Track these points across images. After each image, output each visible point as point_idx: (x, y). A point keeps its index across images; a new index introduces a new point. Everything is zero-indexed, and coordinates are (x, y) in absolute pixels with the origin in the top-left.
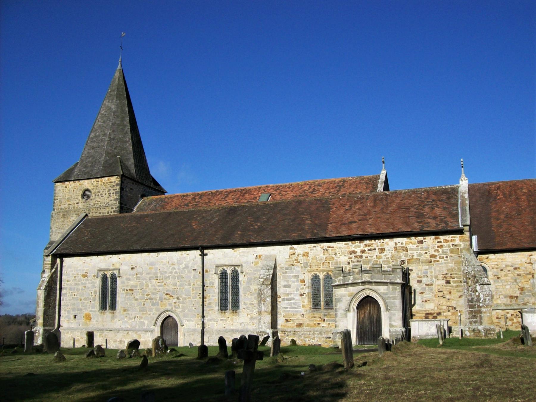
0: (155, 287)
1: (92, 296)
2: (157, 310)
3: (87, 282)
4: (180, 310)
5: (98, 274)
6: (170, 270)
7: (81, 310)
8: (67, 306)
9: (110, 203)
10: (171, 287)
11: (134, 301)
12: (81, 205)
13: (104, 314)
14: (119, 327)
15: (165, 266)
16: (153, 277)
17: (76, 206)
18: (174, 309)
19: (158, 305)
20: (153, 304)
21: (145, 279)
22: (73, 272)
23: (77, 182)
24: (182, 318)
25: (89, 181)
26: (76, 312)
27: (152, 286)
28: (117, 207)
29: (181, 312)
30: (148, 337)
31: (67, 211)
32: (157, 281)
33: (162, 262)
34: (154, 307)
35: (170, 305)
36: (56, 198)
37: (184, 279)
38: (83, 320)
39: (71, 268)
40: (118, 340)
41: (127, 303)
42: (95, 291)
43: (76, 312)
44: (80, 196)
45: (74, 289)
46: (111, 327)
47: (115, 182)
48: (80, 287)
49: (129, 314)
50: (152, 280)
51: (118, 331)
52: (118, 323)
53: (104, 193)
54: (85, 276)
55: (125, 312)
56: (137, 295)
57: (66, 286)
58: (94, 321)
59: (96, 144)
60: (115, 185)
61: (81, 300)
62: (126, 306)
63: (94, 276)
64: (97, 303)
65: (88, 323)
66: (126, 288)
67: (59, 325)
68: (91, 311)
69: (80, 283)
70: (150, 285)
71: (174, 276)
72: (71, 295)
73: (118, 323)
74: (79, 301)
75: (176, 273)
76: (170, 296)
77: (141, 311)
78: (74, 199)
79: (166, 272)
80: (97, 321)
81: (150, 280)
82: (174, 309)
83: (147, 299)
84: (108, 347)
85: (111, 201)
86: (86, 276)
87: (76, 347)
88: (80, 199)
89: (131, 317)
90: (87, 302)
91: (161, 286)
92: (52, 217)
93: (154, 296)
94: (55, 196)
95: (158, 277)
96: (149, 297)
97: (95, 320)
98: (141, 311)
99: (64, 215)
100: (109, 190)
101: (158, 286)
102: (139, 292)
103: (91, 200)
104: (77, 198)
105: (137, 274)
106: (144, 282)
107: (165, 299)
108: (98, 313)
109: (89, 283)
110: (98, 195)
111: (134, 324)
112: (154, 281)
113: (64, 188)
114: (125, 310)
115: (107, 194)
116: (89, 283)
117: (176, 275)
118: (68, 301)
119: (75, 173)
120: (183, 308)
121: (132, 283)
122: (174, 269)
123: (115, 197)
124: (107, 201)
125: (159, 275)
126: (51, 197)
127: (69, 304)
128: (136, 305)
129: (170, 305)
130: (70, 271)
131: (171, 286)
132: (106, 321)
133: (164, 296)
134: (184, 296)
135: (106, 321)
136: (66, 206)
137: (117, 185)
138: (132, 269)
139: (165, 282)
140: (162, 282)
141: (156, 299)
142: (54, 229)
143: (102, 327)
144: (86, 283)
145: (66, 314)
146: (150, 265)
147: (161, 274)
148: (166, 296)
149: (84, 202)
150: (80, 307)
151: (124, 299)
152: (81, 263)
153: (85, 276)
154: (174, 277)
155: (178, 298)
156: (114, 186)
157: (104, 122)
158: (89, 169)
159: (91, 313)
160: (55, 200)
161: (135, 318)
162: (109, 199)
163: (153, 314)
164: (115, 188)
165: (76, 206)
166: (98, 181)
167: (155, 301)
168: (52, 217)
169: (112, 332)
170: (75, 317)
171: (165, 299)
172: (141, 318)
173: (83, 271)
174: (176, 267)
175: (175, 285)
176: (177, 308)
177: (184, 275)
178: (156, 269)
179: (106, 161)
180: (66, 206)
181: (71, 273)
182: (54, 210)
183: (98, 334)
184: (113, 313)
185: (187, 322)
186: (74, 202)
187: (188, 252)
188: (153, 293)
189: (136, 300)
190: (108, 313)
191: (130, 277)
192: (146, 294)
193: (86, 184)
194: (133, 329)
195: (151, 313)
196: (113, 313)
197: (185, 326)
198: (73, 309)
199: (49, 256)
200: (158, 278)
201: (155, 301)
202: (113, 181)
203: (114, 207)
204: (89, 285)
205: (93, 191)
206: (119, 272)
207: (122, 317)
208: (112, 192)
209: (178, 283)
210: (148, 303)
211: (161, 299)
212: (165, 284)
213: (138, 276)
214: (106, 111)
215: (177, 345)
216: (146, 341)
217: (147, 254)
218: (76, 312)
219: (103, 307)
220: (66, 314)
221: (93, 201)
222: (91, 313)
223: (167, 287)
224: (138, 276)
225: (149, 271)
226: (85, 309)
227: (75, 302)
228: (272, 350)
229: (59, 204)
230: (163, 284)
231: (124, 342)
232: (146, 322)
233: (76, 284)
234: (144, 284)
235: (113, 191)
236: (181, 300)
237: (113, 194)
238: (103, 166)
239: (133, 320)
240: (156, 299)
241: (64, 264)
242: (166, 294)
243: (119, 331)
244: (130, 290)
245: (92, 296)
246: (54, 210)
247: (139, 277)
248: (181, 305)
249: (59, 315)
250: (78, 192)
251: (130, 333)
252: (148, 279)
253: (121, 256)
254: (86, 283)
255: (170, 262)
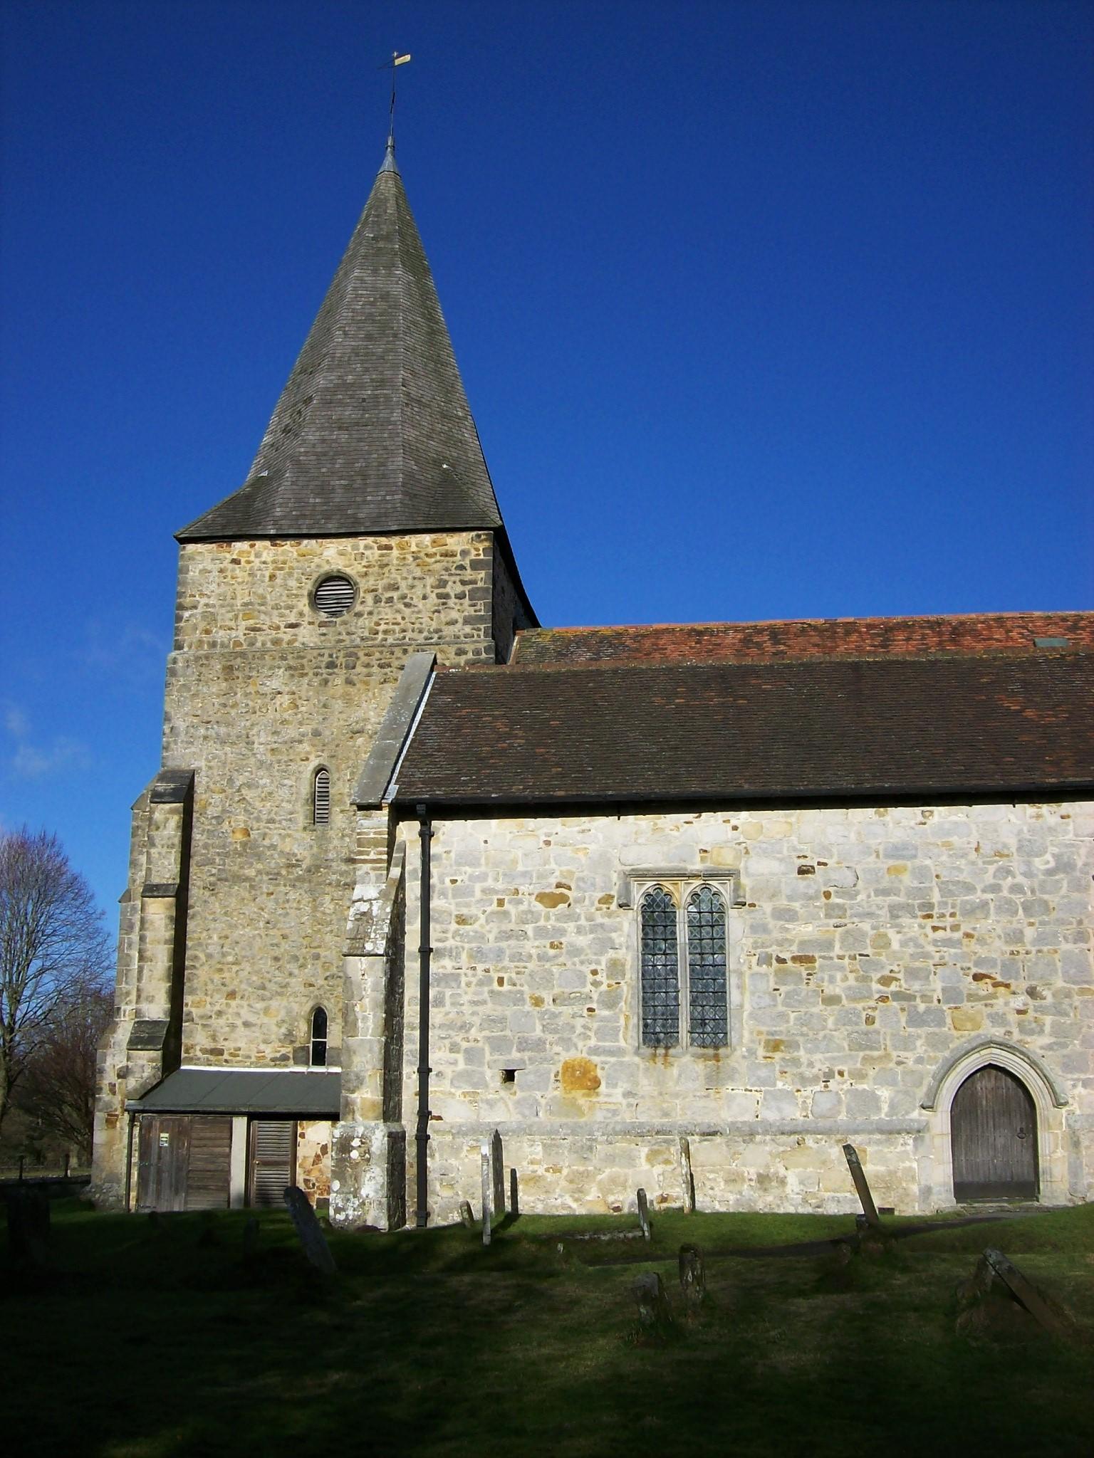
0: (917, 945)
1: (596, 984)
2: (936, 1042)
3: (570, 927)
4: (1046, 1040)
5: (626, 889)
6: (989, 879)
7: (539, 1045)
8: (465, 1027)
9: (449, 631)
10: (997, 949)
11: (818, 1008)
12: (307, 635)
13: (667, 1064)
14: (749, 1118)
15: (961, 863)
16: (908, 909)
17: (286, 635)
18: (1016, 1035)
19: (941, 1023)
20: (916, 1020)
21: (870, 915)
22: (490, 883)
23: (288, 546)
24: (1055, 1072)
25: (347, 543)
26: (515, 1055)
27: (904, 944)
28: (482, 646)
29: (1049, 1047)
30: (903, 1156)
31: (243, 655)
32: (930, 923)
33: (948, 845)
34: (923, 1031)
35: (998, 1019)
36: (187, 601)
37: (1054, 915)
38: (554, 1092)
39: (474, 863)
40: (752, 1172)
41: (783, 1017)
42: (615, 968)
43: (515, 1055)
44: (305, 601)
45: (500, 954)
46: (709, 1119)
47: (464, 553)
48: (531, 946)
49: (796, 1062)
50: (905, 920)
51: (749, 1133)
52: (740, 1102)
53: (419, 591)
54: (551, 900)
55: (778, 1055)
56: (832, 980)
57: (450, 943)
58: (612, 1094)
59: (349, 413)
60: (467, 563)
61: (538, 1002)
62: (783, 1028)
63: (607, 899)
64: (627, 1018)
65: (582, 1101)
66: (774, 950)
67: (424, 1115)
68: (595, 1051)
69: (529, 929)
70: (895, 939)
71: (1009, 902)
72: (481, 983)
73: (740, 1102)
74: (528, 1007)
75: (1017, 889)
76: (996, 985)
77: (856, 1046)
78: (276, 607)
79: (970, 888)
80: (628, 1094)
81: (894, 917)
82: (1016, 1035)
83: (884, 999)
84: (698, 1205)
85: (454, 622)
86: (563, 899)
87: (705, 1203)
88: (307, 610)
89: (809, 1073)
90: (567, 1010)
91: (949, 943)
92: (173, 673)
93: (916, 986)
94: (181, 595)
95: (931, 906)
96: (893, 987)
97: (619, 1091)
98: (856, 1046)
99: (229, 669)
100: (443, 584)
101: (935, 943)
102: (842, 968)
103: (359, 615)
104: (290, 608)
105: (827, 895)
106: (866, 926)
107: (972, 997)
108: (631, 1058)
109: (579, 931)
110: (390, 600)
111: (825, 1103)
112: (913, 925)
113: (226, 564)
114: (775, 1046)
115: (433, 598)
116: (579, 931)
117: (1018, 899)
118: (467, 1009)
119: (278, 512)
120: (1058, 1030)
121: (806, 930)
122: (1008, 872)
123: (471, 611)
124: (434, 625)
125: (936, 897)
126: (165, 603)
127: (476, 1020)
128: (830, 1022)
129: (998, 1019)
130: (472, 878)
131: (998, 943)
132: (677, 1095)
133: (968, 983)
134: (1059, 983)
135: (677, 1095)
136: (240, 634)
137: (475, 565)
138: (802, 871)
139: (965, 928)
140: (955, 928)
141: (926, 998)
142: (181, 724)
143: (658, 1121)
144: (563, 932)
145: (461, 1066)
146: (887, 856)
147: (945, 892)
148: (974, 985)
149: (321, 625)
150: (538, 1032)
151: (767, 1000)
152: (530, 844)
153: (551, 900)
154: (1008, 908)
155: (1032, 992)
156: (462, 567)
157: (369, 337)
158: (338, 497)
159: (595, 1059)
160: (181, 607)
161: (828, 1077)
162: (444, 617)
163: (919, 1060)
164: (469, 574)
165: (287, 638)
166: (389, 548)
167: (922, 1007)
168: (173, 673)
169: (718, 1139)
170: (509, 1076)
171: (972, 997)
172: (859, 1076)
173: (541, 876)
174: (1016, 864)
175: (1017, 937)
176: (1032, 1032)
177: (1053, 900)
178: (921, 873)
179: (410, 475)
180: (240, 634)
181: (478, 887)
182: (179, 647)
183: (644, 1151)
184: (717, 1058)
185: (1080, 1090)
186: (276, 620)
187: (1066, 807)
188: (912, 974)
189: (831, 1000)
190: (687, 1062)
191: (796, 905)
192: (876, 976)
193: (333, 554)
194: (822, 1123)
195: (910, 1057)
196: (717, 1058)
197: (1075, 1107)
198: (498, 1045)
199: (378, 807)
200: (935, 912)
201: (922, 1007)
202: (458, 549)
203: (469, 648)
204: (583, 941)
205: (363, 584)
206: (738, 886)
207: (763, 1073)
208: (453, 588)
209: (1030, 933)
210: (892, 1020)
211: (952, 995)
212: (968, 935)
213: (835, 900)
214: (372, 304)
215: (1029, 1187)
216: (892, 1173)
217: (870, 812)
218: (514, 1057)
219: (657, 1033)
220: (461, 1066)
221: (365, 622)
222: (595, 1059)
223: (978, 948)
224: (835, 900)
225: (885, 883)
226: (567, 1043)
227: (509, 1011)
228: (1036, 1204)
229: (202, 625)
230: (957, 935)
231: (782, 1182)
232: (885, 1093)
233: (507, 935)
234: (864, 934)
235: (459, 588)
236: (1050, 999)
237: (460, 596)
238: (405, 493)
239: (819, 1087)
240: (926, 998)
241: (435, 849)
242: (977, 977)
243: (752, 1134)
244: (794, 959)
245: (596, 984)
246: (179, 647)
247: (841, 907)
248: (1048, 1020)
249: (424, 1071)
250: (292, 583)
251: (810, 1141)
252: (884, 912)
253: (743, 818)
254: (563, 932)
255: (987, 848)
